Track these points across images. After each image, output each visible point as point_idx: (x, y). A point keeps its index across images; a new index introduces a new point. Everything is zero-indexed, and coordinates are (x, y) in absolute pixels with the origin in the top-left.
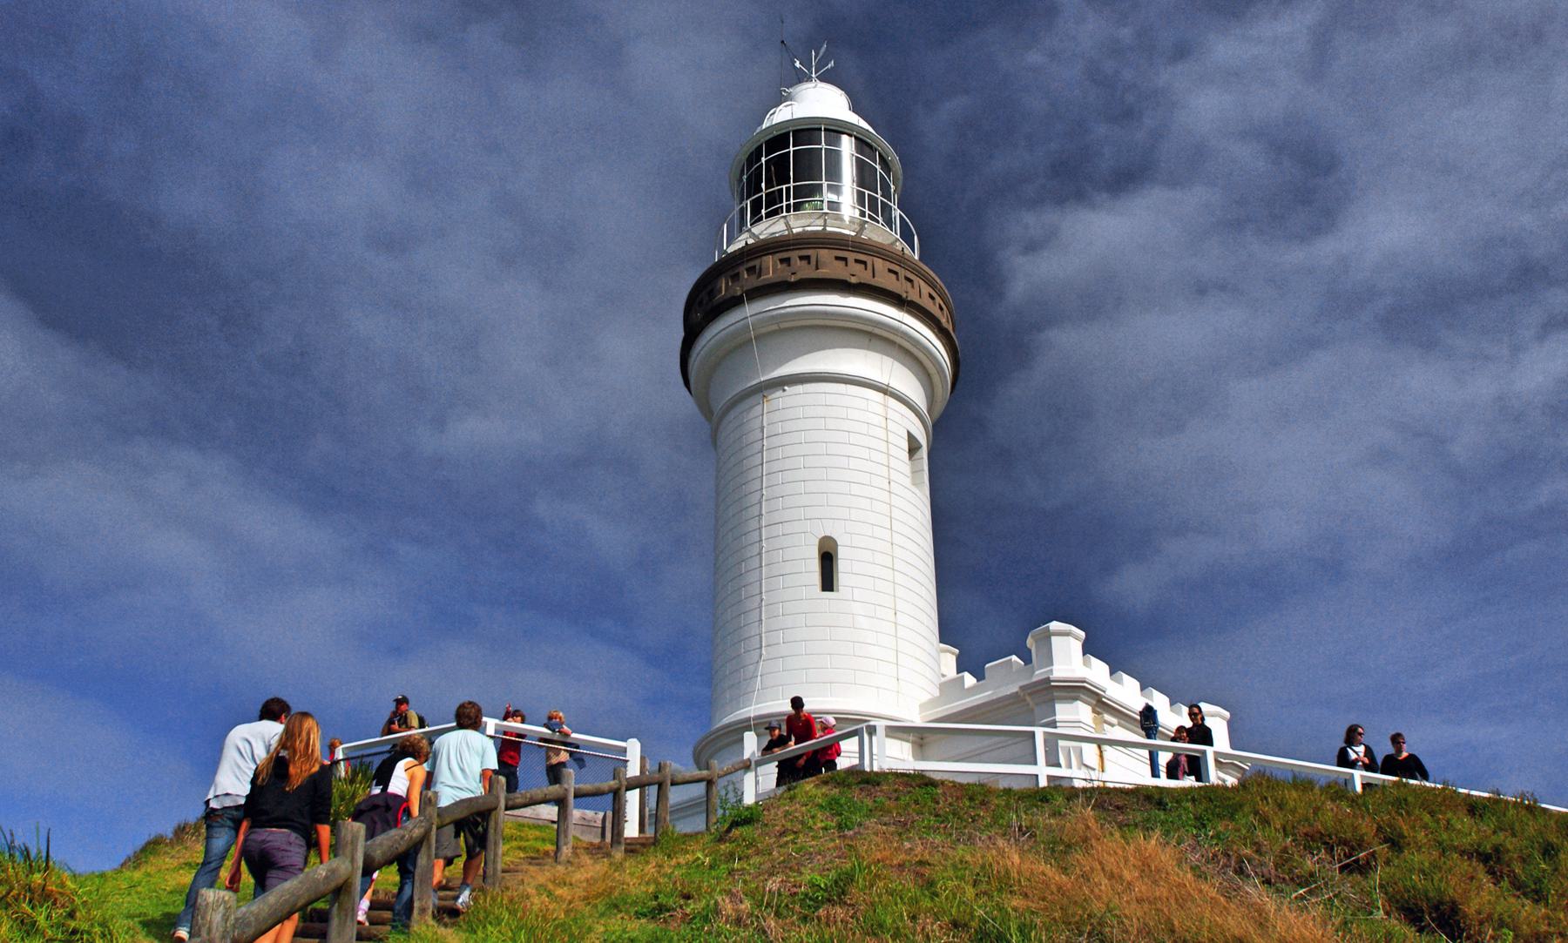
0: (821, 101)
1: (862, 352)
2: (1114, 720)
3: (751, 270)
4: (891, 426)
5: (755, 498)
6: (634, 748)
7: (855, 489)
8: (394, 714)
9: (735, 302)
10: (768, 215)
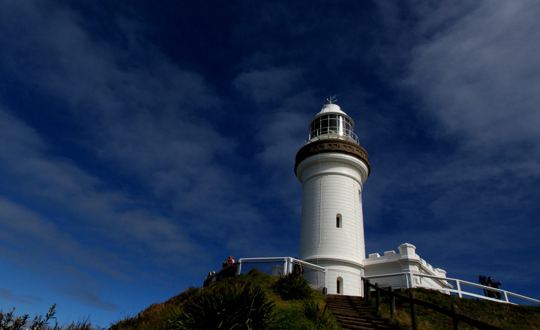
0: (334, 108)
3: (320, 146)
6: (344, 251)
7: (346, 202)
9: (316, 153)
10: (322, 134)
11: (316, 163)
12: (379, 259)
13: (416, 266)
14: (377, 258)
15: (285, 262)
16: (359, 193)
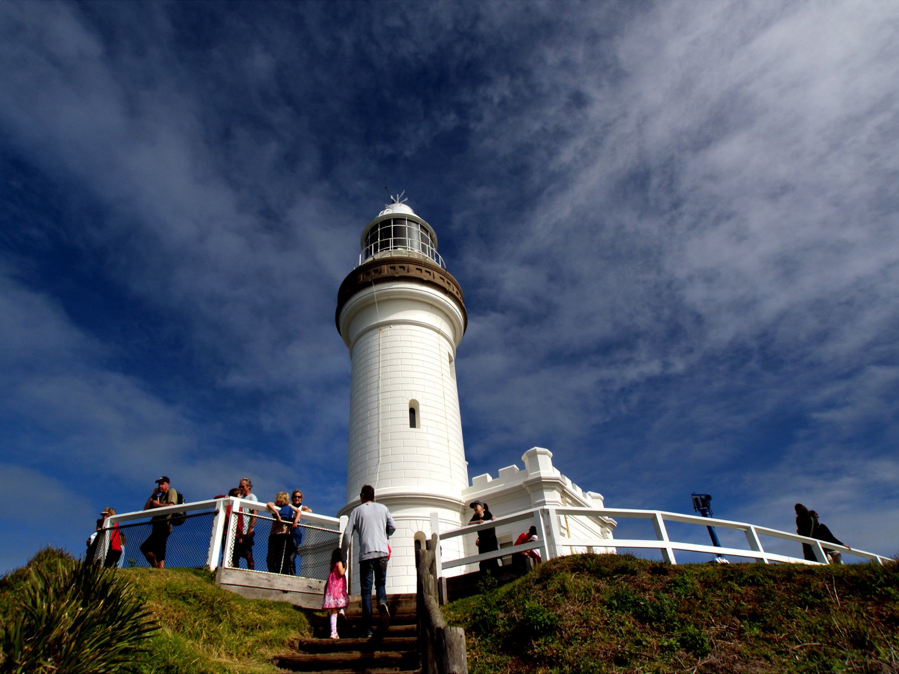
0: (402, 209)
1: (428, 313)
2: (570, 501)
3: (376, 271)
4: (442, 349)
5: (376, 378)
6: (421, 473)
8: (159, 490)
9: (368, 285)
11: (369, 306)
12: (491, 484)
13: (555, 491)
14: (488, 485)
15: (217, 513)
16: (450, 362)
